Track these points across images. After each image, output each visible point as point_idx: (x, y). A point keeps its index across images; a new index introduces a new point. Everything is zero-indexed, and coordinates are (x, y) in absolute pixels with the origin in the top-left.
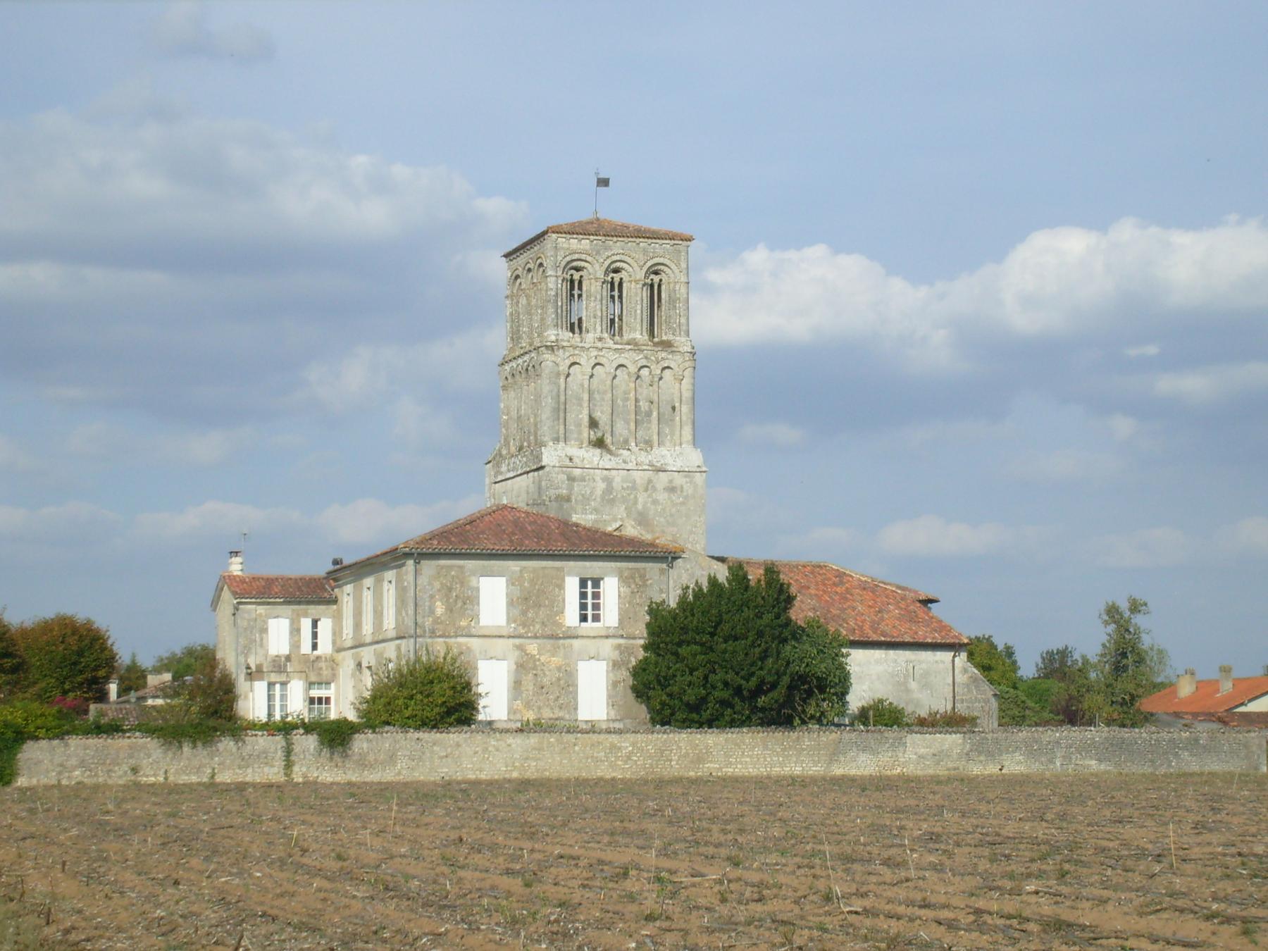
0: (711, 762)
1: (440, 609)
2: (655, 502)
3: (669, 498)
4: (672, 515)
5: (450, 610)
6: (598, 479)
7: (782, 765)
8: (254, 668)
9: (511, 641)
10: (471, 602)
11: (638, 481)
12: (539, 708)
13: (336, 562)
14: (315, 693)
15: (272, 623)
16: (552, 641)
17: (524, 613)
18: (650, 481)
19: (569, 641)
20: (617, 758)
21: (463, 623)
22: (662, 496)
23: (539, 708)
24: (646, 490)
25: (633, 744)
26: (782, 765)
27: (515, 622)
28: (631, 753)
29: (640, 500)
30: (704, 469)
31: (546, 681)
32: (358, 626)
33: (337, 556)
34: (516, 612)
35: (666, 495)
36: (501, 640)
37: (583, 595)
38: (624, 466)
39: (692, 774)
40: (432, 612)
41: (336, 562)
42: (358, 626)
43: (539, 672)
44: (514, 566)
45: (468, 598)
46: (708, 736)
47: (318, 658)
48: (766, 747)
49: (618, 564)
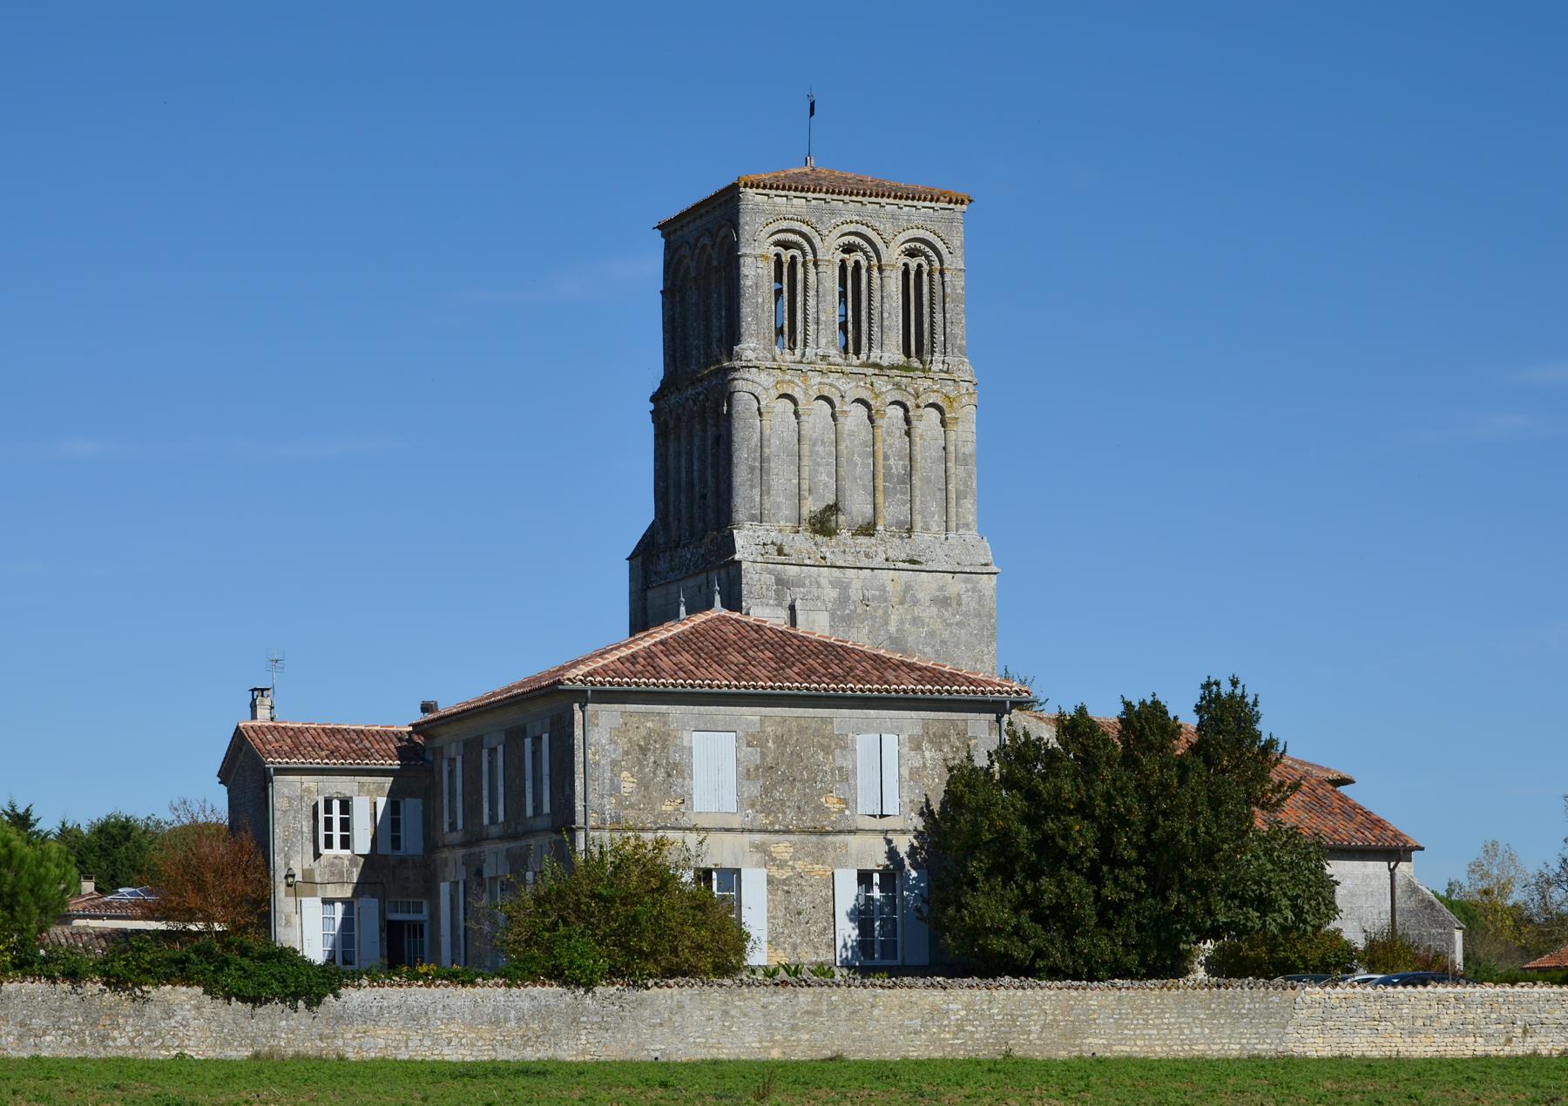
0: (1095, 1035)
1: (628, 784)
2: (916, 621)
3: (941, 616)
4: (943, 642)
5: (644, 784)
6: (824, 582)
7: (1210, 1041)
8: (299, 878)
9: (747, 837)
10: (681, 774)
11: (890, 587)
12: (795, 947)
13: (426, 708)
14: (876, 878)
15: (864, 744)
16: (814, 838)
17: (767, 791)
18: (908, 588)
19: (841, 837)
20: (942, 1028)
21: (667, 808)
22: (928, 613)
23: (795, 947)
24: (902, 603)
25: (967, 1007)
26: (1210, 1041)
27: (753, 806)
28: (965, 1019)
29: (894, 618)
30: (994, 569)
31: (805, 903)
32: (473, 810)
33: (428, 699)
34: (754, 789)
35: (934, 610)
36: (729, 837)
37: (345, 825)
38: (865, 562)
39: (1063, 1054)
40: (615, 788)
41: (426, 708)
42: (473, 810)
43: (793, 888)
44: (750, 715)
45: (676, 765)
46: (1089, 993)
47: (402, 861)
48: (1182, 1013)
49: (923, 714)
